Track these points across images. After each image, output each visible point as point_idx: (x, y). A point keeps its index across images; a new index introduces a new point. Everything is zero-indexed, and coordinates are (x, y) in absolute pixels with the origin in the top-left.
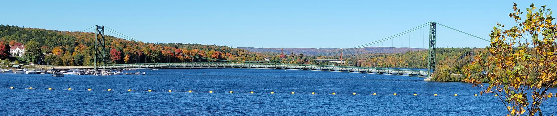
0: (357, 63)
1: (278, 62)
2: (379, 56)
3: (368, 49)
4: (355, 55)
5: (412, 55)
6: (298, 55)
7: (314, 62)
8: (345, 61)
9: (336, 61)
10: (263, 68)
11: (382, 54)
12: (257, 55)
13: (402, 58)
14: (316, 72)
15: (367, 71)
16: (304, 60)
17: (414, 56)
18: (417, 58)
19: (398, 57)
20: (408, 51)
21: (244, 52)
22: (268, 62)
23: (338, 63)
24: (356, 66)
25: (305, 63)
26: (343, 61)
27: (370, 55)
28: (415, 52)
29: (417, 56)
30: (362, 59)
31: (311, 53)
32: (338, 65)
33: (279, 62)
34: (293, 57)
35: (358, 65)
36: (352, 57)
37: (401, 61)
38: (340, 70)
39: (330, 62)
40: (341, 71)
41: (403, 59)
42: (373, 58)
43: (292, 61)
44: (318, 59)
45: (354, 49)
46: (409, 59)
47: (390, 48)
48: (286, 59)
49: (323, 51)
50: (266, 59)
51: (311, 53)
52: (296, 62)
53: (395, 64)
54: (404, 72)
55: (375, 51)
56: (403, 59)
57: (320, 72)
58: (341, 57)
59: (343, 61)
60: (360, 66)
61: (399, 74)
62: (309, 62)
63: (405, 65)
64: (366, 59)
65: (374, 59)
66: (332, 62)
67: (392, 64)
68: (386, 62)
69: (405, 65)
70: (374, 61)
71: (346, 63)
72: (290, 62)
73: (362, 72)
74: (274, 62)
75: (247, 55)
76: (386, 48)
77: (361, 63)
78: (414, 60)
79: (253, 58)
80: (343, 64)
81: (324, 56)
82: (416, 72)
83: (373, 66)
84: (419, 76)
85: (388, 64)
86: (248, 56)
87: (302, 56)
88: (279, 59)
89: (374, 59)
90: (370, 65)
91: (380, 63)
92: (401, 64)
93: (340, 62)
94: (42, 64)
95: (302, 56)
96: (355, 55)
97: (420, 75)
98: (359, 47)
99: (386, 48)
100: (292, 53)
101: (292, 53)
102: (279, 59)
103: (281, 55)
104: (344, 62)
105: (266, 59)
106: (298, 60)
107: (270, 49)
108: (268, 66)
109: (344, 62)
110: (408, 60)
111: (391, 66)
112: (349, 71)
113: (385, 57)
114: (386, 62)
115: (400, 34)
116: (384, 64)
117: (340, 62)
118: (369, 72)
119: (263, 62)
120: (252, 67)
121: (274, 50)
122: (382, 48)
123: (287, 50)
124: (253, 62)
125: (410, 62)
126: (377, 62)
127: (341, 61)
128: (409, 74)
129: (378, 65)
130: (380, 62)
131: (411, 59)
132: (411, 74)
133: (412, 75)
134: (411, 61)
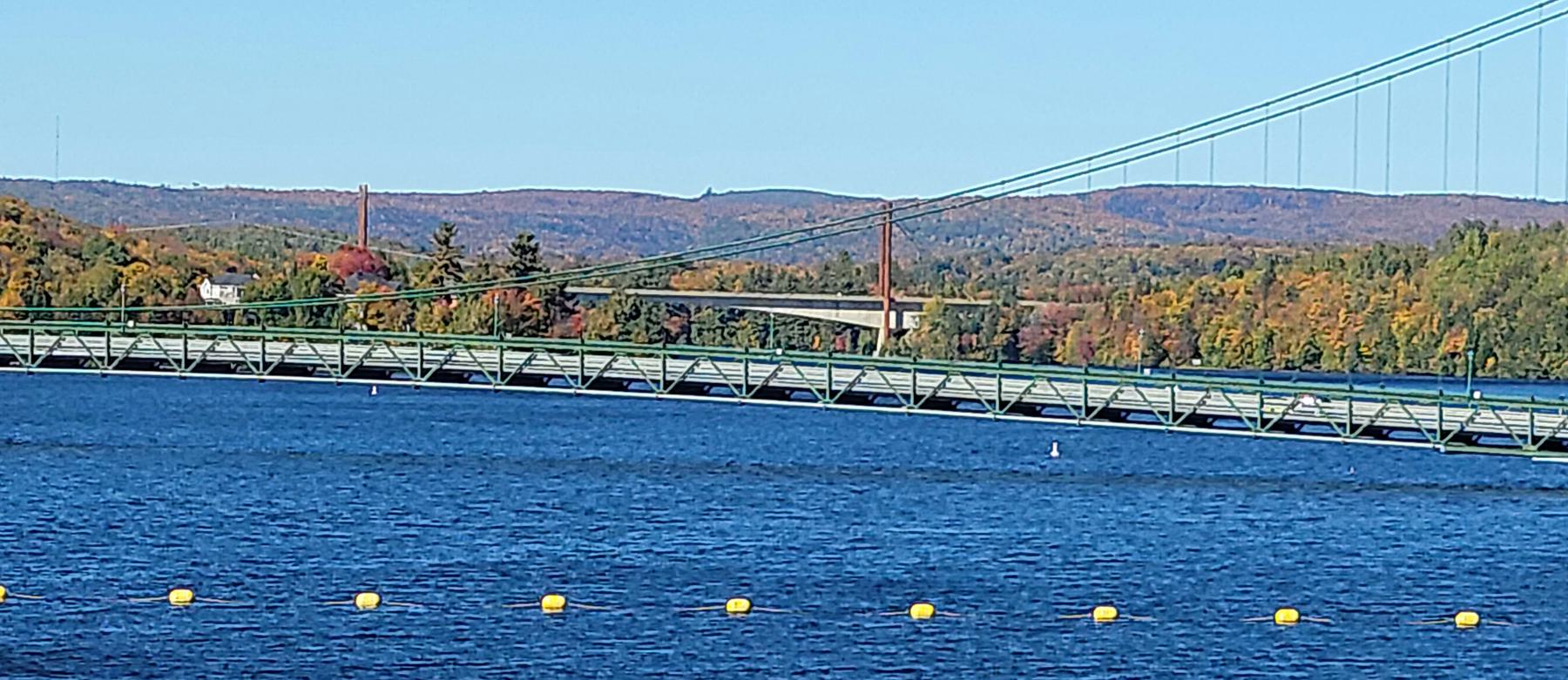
0: (1025, 331)
1: (317, 315)
2: (1219, 266)
3: (1124, 202)
4: (1007, 260)
5: (1493, 263)
6: (500, 249)
7: (636, 314)
8: (920, 306)
9: (837, 305)
10: (149, 364)
11: (1246, 251)
12: (135, 251)
13: (1412, 287)
14: (710, 412)
15: (1425, 425)
16: (551, 301)
17: (1519, 271)
18: (1541, 291)
19: (1380, 277)
20: (1469, 226)
21: (17, 219)
22: (229, 316)
23: (855, 330)
24: (1012, 352)
25: (557, 329)
26: (900, 308)
27: (1139, 254)
28: (1525, 234)
29: (1546, 268)
30: (1062, 295)
31: (623, 236)
32: (854, 341)
33: (321, 309)
34: (453, 268)
35: (1028, 347)
36: (986, 272)
37: (1401, 317)
38: (833, 393)
39: (787, 321)
40: (440, 375)
41: (1425, 294)
42: (1166, 281)
43: (438, 308)
44: (684, 287)
45: (1006, 201)
46: (1472, 296)
47: (1319, 199)
48: (388, 290)
49: (727, 219)
50: (208, 291)
51: (623, 236)
52: (473, 314)
53: (1349, 338)
54: (1395, 415)
55: (1191, 225)
56: (1425, 294)
57: (734, 414)
58: (884, 272)
59: (900, 308)
60: (1045, 356)
61: (1354, 428)
62: (596, 319)
63: (1441, 351)
64: (1096, 297)
65: (1173, 295)
66: (807, 320)
67: (1330, 342)
68: (1271, 323)
69: (1441, 351)
70: (1168, 311)
71: (927, 328)
72: (419, 316)
73: (1030, 409)
74: (284, 312)
75: (43, 253)
76: (1286, 199)
77: (1057, 326)
78: (1517, 304)
79: (93, 279)
80: (901, 333)
81: (741, 266)
82: (1504, 415)
83: (1158, 357)
84: (1531, 449)
85: (1293, 340)
86: (57, 261)
87: (526, 257)
88: (330, 287)
89: (1173, 295)
90: (1137, 347)
91: (1225, 329)
92: (1401, 338)
93: (875, 319)
94: (374, 392)
95: (526, 257)
96: (1007, 260)
97: (1535, 440)
98: (1007, 187)
99: (1283, 196)
100: (442, 234)
101: (442, 234)
102: (330, 287)
103: (347, 255)
104: (906, 314)
105: (208, 291)
106: (493, 299)
107: (266, 200)
108: (198, 347)
109: (906, 314)
110: (1463, 308)
111: (1317, 357)
112: (918, 398)
113: (1270, 280)
114: (1271, 323)
115: (1363, 79)
116: (1258, 337)
117: (875, 319)
118: (1089, 410)
119: (181, 315)
120: (51, 361)
121: (295, 204)
122: (1252, 197)
123: (412, 206)
124: (89, 313)
125: (1486, 325)
126: (1198, 322)
127: (877, 306)
128: (1444, 434)
129: (1203, 343)
130: (1226, 318)
131: (1489, 299)
132: (1456, 428)
133: (1464, 437)
134: (1491, 313)
